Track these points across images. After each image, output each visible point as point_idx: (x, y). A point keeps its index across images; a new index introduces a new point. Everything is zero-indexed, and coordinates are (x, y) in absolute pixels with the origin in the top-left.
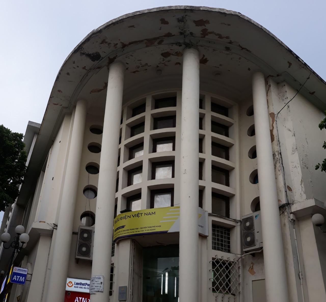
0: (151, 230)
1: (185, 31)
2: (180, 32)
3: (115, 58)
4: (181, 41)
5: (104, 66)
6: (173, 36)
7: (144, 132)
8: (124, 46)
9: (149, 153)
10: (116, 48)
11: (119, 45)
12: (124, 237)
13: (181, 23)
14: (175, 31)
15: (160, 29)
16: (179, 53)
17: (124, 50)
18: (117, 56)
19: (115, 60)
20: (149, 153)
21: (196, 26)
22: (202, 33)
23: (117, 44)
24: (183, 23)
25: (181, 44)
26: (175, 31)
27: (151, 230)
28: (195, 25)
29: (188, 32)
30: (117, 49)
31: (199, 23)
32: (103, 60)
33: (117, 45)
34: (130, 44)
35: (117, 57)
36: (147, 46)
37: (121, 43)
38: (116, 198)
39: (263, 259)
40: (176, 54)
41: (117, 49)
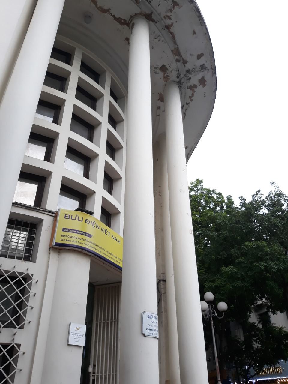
0: (116, 261)
1: (191, 73)
2: (189, 70)
3: (153, 21)
4: (182, 76)
5: (140, 9)
6: (184, 65)
7: (70, 130)
8: (168, 27)
9: (64, 178)
10: (165, 17)
11: (169, 22)
12: (89, 252)
13: (200, 68)
14: (189, 66)
15: (190, 55)
16: (168, 78)
17: (164, 29)
18: (156, 23)
19: (151, 22)
20: (64, 178)
21: (199, 80)
22: (192, 86)
23: (170, 19)
24: (200, 70)
25: (180, 77)
26: (189, 66)
27: (116, 261)
28: (200, 79)
29: (190, 76)
30: (163, 19)
31: (203, 81)
32: (147, 3)
33: (169, 20)
34: (172, 33)
35: (155, 23)
36: (172, 51)
37: (172, 24)
38: (100, 220)
39: (116, 321)
40: (166, 76)
41: (163, 19)
